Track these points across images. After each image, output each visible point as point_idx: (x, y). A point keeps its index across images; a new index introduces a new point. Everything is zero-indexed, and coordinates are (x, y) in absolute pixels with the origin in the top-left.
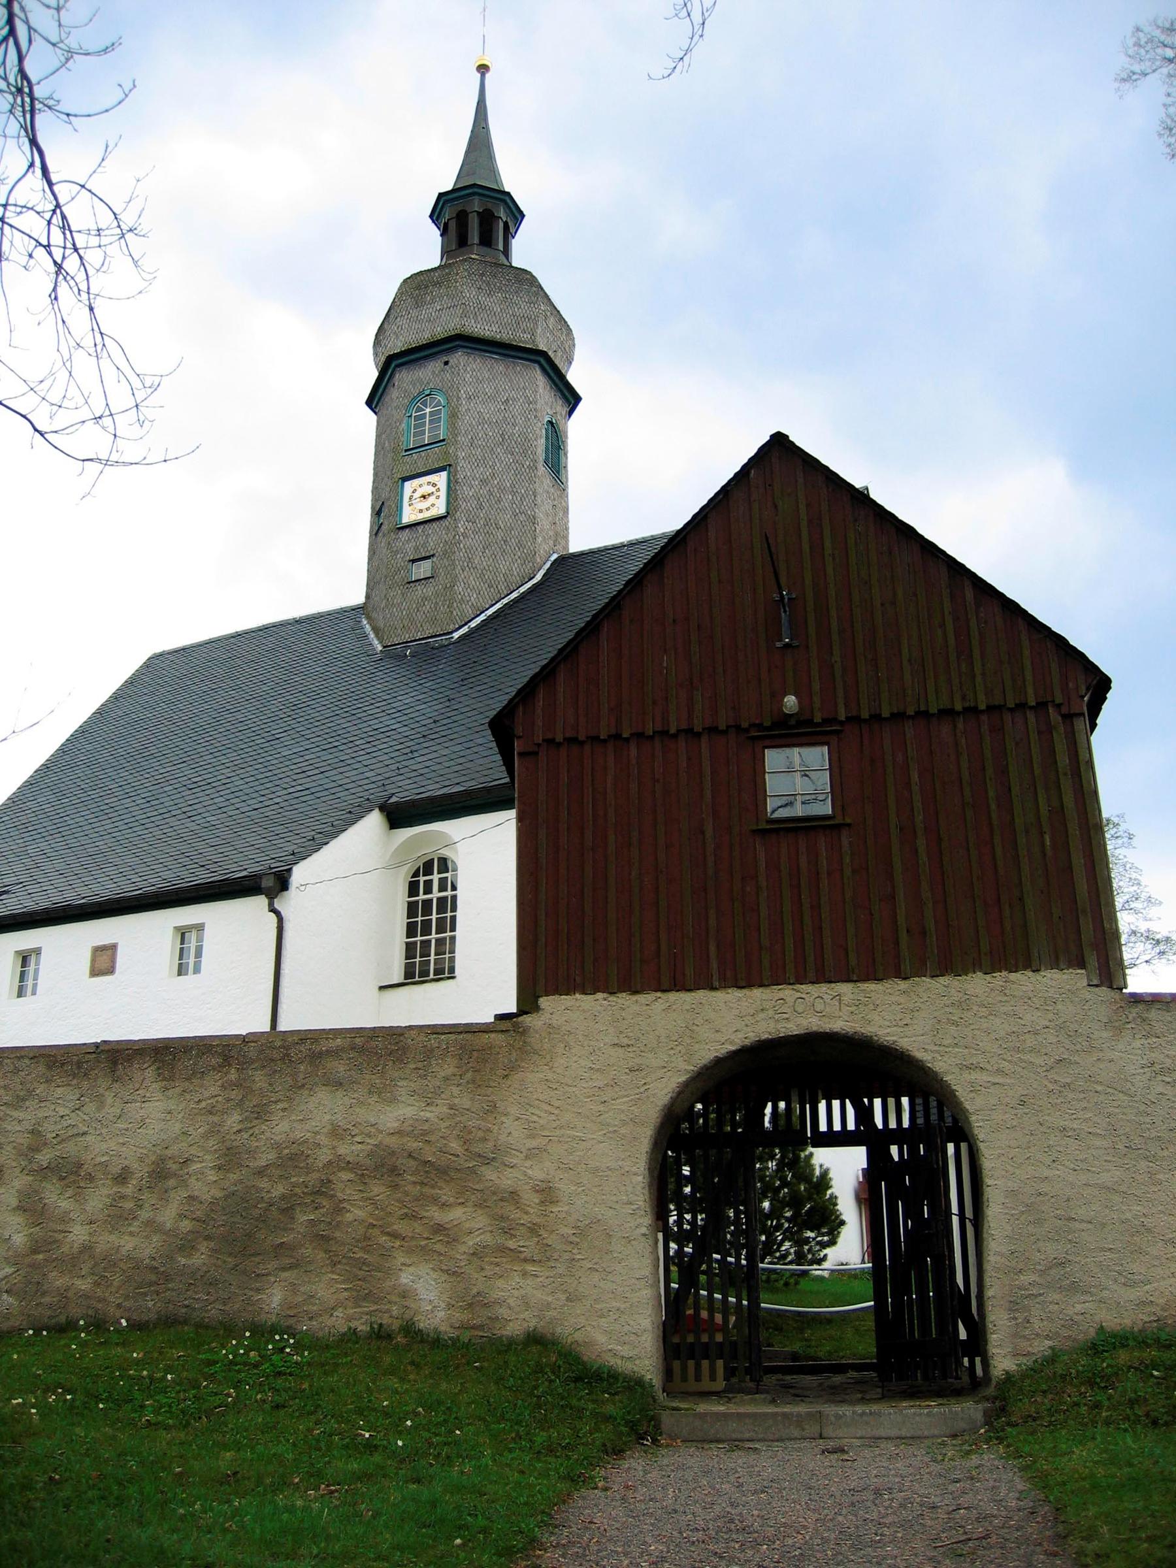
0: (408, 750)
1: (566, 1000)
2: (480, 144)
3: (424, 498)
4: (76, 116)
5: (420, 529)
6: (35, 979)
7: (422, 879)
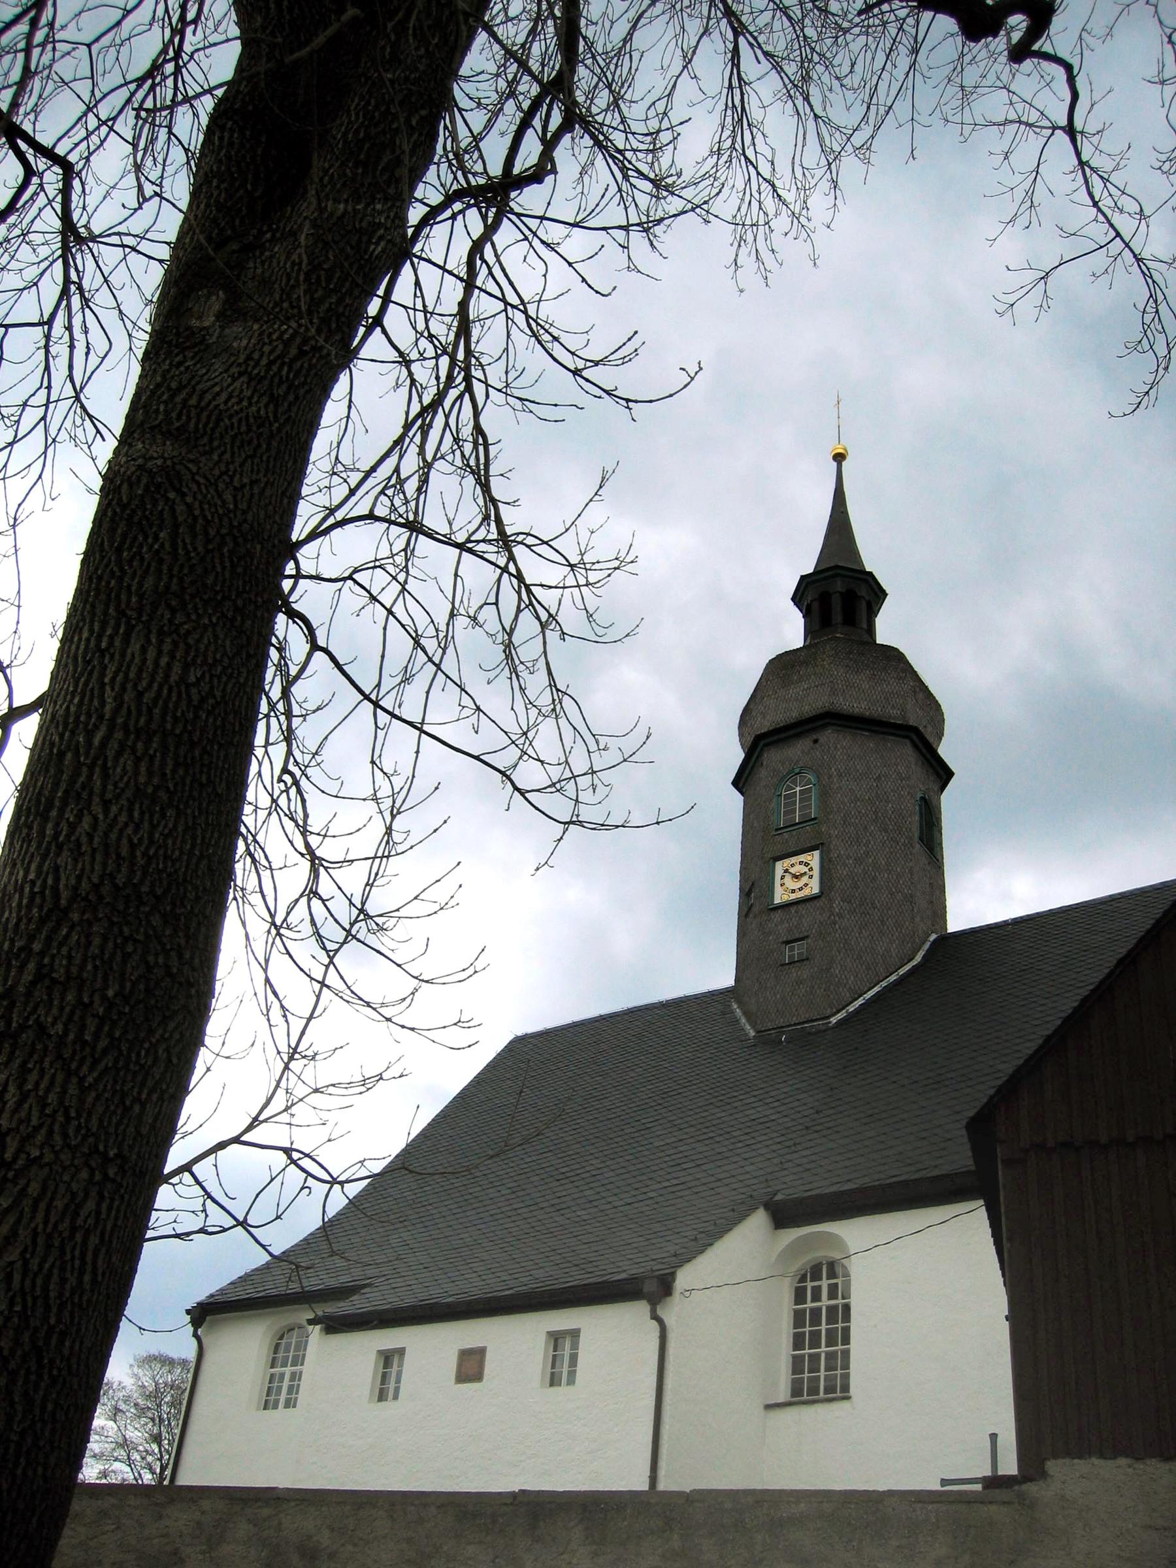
0: (791, 1143)
1: (1081, 1466)
2: (839, 526)
3: (797, 878)
4: (636, 402)
5: (793, 909)
6: (398, 1381)
7: (810, 1285)
